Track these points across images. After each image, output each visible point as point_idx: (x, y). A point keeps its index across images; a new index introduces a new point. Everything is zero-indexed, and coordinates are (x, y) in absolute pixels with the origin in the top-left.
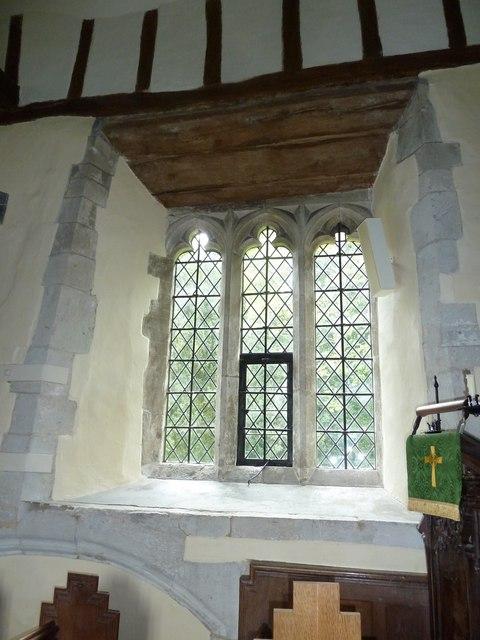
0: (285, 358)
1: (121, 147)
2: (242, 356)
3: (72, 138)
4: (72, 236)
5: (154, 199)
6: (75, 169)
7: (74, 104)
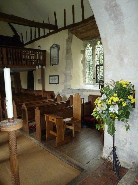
0: (102, 65)
1: (73, 33)
2: (96, 65)
3: (65, 34)
4: (68, 51)
5: (80, 40)
6: (67, 40)
7: (65, 28)
